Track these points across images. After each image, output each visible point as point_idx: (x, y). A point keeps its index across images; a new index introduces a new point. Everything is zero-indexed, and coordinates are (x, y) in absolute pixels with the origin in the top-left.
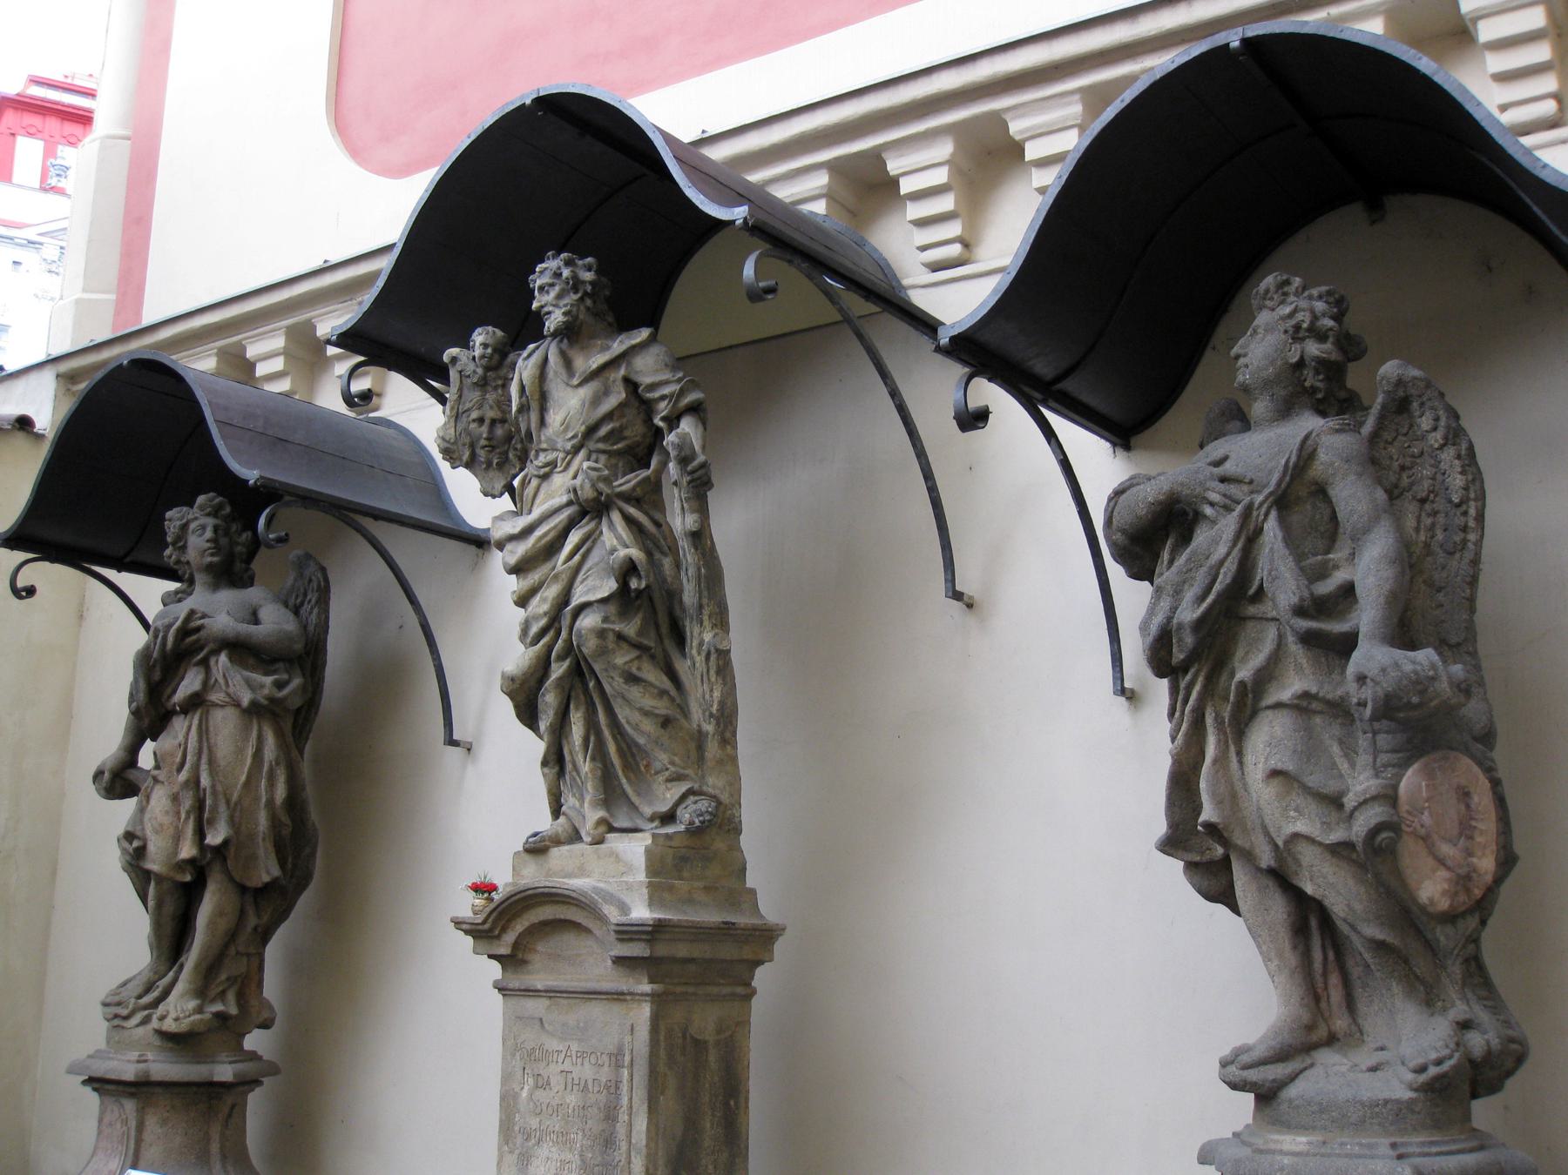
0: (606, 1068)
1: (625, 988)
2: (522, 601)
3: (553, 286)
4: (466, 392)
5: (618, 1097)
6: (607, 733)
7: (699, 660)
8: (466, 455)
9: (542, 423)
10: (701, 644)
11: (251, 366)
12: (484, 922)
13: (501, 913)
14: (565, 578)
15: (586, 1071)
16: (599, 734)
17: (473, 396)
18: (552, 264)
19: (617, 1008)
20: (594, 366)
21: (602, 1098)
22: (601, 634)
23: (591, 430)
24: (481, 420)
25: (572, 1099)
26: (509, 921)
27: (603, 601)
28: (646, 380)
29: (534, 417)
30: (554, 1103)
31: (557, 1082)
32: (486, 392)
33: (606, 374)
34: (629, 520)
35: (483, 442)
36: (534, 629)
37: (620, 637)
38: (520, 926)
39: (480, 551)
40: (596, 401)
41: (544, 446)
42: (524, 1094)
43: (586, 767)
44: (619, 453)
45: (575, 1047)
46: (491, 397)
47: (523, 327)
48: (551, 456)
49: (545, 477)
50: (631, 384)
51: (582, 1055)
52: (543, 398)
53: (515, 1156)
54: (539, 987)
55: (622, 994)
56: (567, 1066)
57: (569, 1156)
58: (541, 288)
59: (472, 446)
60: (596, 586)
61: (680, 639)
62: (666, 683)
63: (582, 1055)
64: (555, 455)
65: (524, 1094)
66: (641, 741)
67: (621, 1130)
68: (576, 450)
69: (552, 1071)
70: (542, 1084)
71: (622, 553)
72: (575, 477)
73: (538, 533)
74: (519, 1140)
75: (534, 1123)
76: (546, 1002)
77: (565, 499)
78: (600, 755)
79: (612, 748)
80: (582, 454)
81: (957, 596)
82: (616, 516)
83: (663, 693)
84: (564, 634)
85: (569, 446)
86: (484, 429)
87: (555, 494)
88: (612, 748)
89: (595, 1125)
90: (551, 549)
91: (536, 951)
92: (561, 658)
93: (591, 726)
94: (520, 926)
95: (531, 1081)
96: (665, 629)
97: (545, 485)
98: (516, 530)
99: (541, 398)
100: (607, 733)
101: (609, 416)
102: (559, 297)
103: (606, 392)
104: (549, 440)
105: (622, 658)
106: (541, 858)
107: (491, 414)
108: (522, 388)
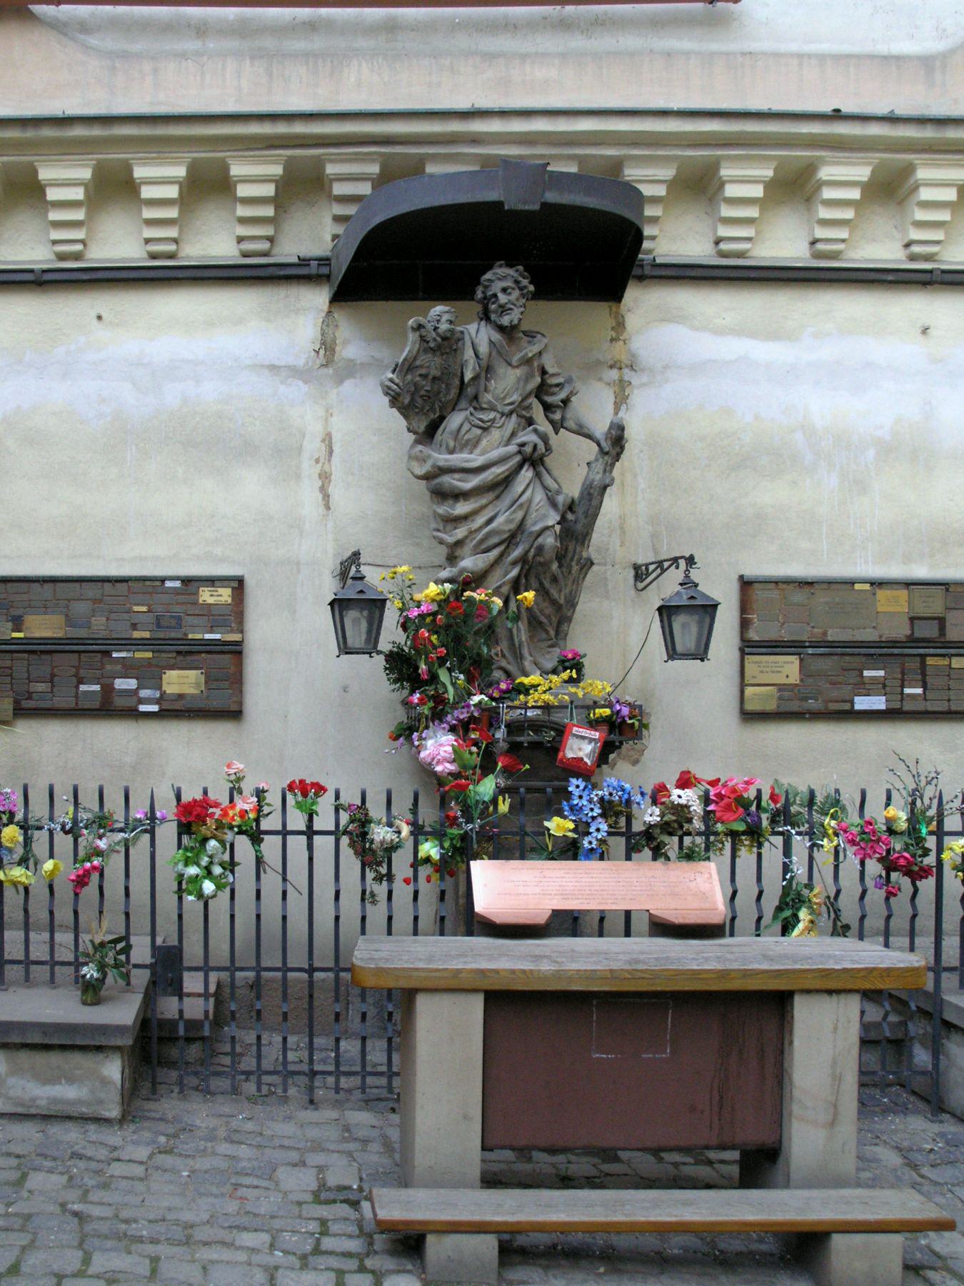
28: (550, 370)
35: (423, 393)
46: (438, 360)
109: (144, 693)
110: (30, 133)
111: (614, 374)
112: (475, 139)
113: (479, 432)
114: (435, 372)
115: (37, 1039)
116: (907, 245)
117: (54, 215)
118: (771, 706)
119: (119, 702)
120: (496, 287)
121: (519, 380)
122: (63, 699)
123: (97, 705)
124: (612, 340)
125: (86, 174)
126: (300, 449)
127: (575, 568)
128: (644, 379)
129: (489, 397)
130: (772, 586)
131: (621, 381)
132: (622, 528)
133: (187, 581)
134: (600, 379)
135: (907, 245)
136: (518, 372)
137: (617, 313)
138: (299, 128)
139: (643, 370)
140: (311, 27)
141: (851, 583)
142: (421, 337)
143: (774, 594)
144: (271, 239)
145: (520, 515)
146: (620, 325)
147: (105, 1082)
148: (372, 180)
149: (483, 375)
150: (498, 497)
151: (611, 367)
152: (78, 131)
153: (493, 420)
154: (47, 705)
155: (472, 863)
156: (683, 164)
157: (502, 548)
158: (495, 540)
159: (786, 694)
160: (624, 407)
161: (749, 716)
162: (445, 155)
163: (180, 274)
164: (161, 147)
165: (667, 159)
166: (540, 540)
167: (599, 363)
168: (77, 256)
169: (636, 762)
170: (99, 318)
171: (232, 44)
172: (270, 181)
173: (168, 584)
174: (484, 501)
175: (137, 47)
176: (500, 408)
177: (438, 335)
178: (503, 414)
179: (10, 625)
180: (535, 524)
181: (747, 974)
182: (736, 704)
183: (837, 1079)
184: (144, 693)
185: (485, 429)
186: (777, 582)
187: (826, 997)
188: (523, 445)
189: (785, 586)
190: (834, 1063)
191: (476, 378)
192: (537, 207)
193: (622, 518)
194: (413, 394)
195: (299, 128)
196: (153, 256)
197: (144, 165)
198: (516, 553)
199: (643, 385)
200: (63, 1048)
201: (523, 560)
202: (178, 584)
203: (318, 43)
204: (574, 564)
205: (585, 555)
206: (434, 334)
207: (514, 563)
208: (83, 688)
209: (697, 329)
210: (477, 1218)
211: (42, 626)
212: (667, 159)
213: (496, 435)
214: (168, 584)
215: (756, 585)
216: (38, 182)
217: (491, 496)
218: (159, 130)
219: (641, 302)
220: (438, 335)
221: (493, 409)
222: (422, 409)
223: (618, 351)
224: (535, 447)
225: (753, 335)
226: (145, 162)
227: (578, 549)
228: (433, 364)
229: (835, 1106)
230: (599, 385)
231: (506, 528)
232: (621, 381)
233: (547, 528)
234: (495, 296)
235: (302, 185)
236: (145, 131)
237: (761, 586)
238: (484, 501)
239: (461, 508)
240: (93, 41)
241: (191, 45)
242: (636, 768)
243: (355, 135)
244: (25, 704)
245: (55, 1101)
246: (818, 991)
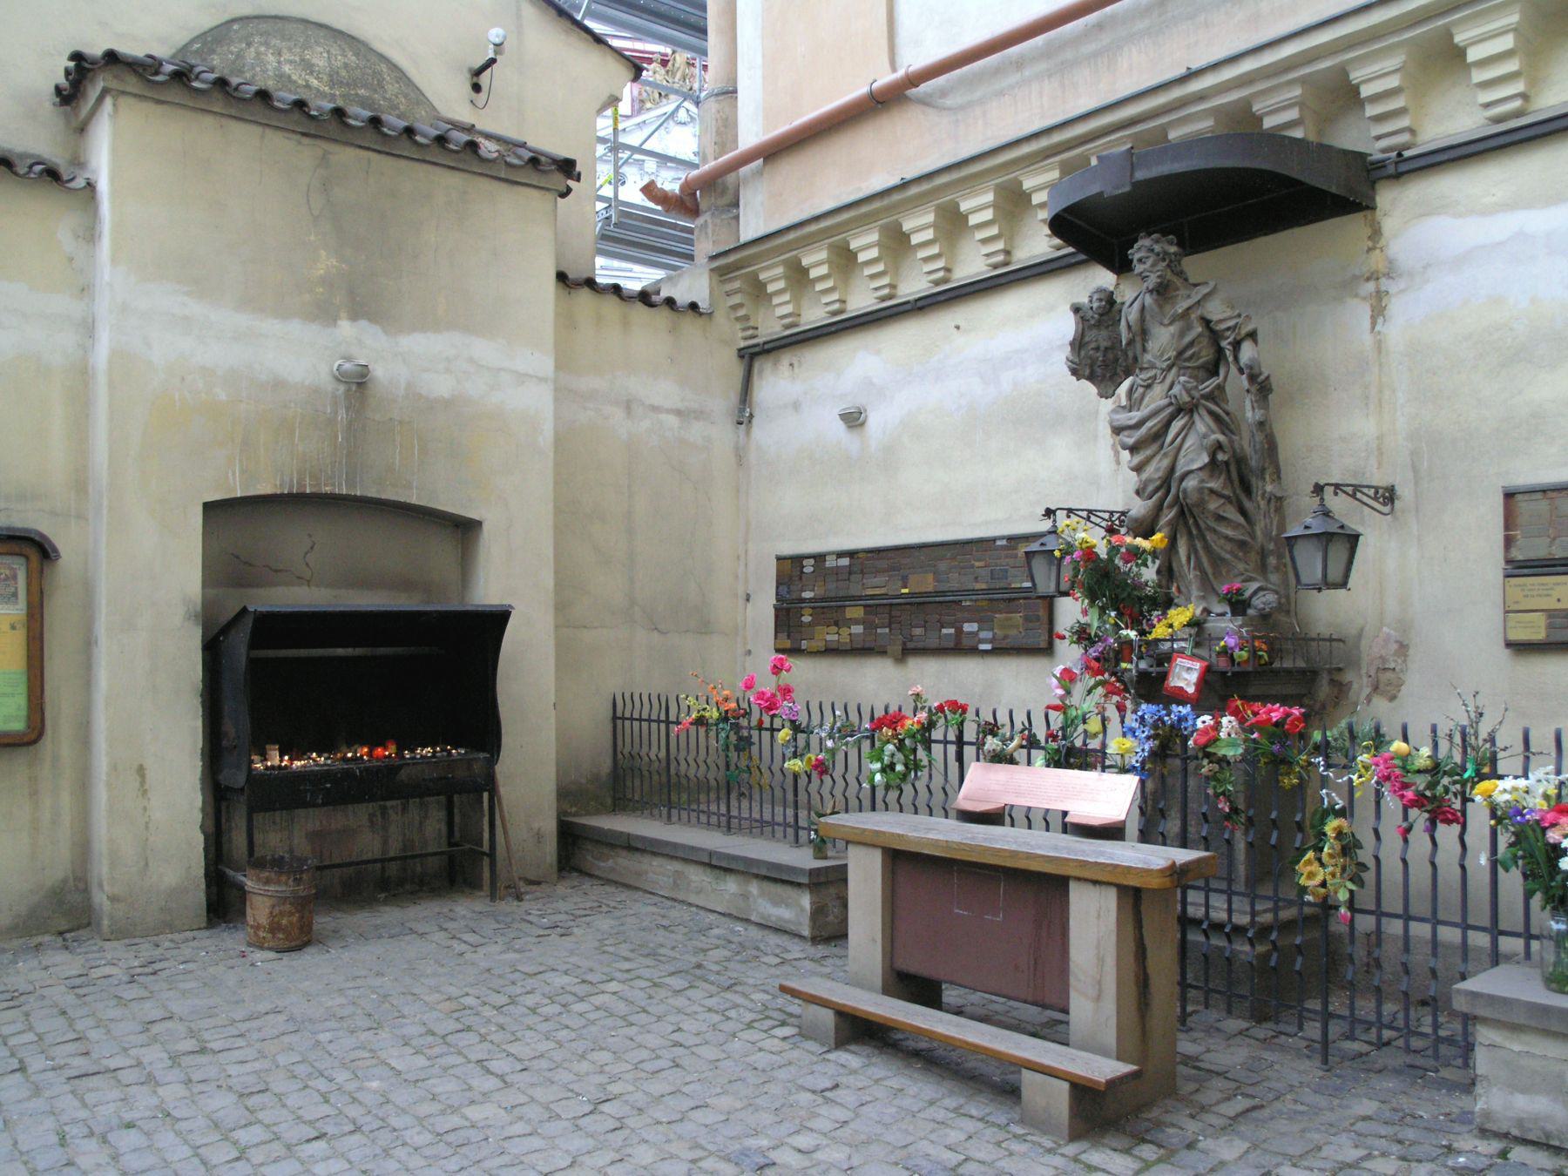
2: (1138, 469)
6: (1201, 552)
7: (1263, 503)
8: (1087, 372)
9: (1144, 350)
11: (805, 271)
14: (1172, 454)
16: (1196, 552)
18: (1144, 242)
22: (1200, 490)
24: (1097, 349)
27: (1200, 469)
28: (1214, 318)
29: (1139, 346)
34: (1211, 413)
36: (1150, 488)
37: (1212, 491)
40: (1182, 334)
43: (1192, 575)
44: (1198, 368)
46: (1104, 333)
48: (1151, 373)
49: (1148, 387)
50: (1207, 322)
58: (1140, 260)
59: (1091, 366)
60: (1194, 457)
61: (1247, 490)
62: (1241, 520)
68: (1170, 368)
71: (1213, 437)
72: (1171, 388)
73: (1149, 424)
77: (1166, 401)
78: (1199, 566)
79: (1205, 560)
80: (1174, 370)
82: (1203, 412)
83: (1237, 526)
84: (1173, 491)
85: (1164, 365)
86: (1100, 356)
87: (1156, 398)
88: (1205, 560)
90: (1158, 436)
92: (1171, 507)
93: (1192, 549)
96: (1236, 483)
98: (1133, 422)
100: (1201, 552)
101: (1191, 344)
102: (1153, 265)
103: (1189, 327)
105: (1213, 505)
108: (1129, 327)
109: (983, 635)
110: (886, 202)
111: (1370, 287)
112: (1201, 97)
114: (1104, 344)
115: (764, 872)
117: (1478, 76)
118: (1540, 635)
119: (966, 642)
121: (1173, 336)
122: (933, 642)
123: (952, 645)
124: (1370, 250)
126: (1097, 412)
128: (1402, 285)
129: (1148, 357)
130: (1539, 496)
131: (1378, 292)
132: (1379, 449)
133: (1010, 539)
134: (1356, 296)
136: (1172, 329)
137: (1373, 220)
138: (1057, 138)
139: (1400, 276)
140: (1100, 27)
141: (994, 540)
143: (1542, 505)
144: (1524, 96)
145: (1166, 462)
146: (1376, 233)
147: (802, 910)
148: (1515, 30)
149: (1138, 339)
151: (1368, 279)
152: (914, 191)
153: (1155, 377)
154: (920, 645)
155: (1137, 778)
156: (785, 263)
157: (1159, 494)
159: (1558, 621)
160: (1380, 320)
161: (1520, 648)
162: (1178, 120)
163: (901, 309)
164: (808, 242)
165: (1290, 83)
167: (1355, 278)
168: (841, 312)
169: (1393, 698)
170: (958, 328)
171: (1042, 66)
172: (1506, 32)
173: (999, 543)
174: (1149, 452)
175: (978, 94)
176: (1158, 364)
179: (900, 583)
181: (1030, 856)
182: (1501, 636)
183: (1101, 960)
184: (983, 635)
186: (1544, 491)
187: (1091, 886)
189: (1554, 494)
190: (1098, 947)
191: (1130, 342)
192: (1127, 189)
193: (1380, 438)
195: (1057, 138)
196: (1498, 120)
199: (1402, 291)
200: (784, 882)
202: (1004, 542)
203: (1106, 39)
208: (944, 631)
209: (1460, 216)
210: (813, 992)
211: (924, 582)
212: (1290, 83)
214: (999, 543)
215: (1519, 497)
216: (1456, 47)
217: (1154, 447)
218: (963, 171)
219: (1394, 203)
221: (1153, 367)
223: (1376, 261)
225: (1529, 205)
226: (965, 197)
228: (1101, 337)
229: (1099, 983)
230: (1355, 301)
232: (1378, 292)
233: (1191, 472)
235: (1013, 203)
236: (955, 175)
237: (1526, 497)
238: (1149, 452)
240: (949, 102)
241: (1014, 78)
242: (1393, 704)
243: (1068, 141)
244: (910, 645)
245: (780, 919)
246: (1086, 880)
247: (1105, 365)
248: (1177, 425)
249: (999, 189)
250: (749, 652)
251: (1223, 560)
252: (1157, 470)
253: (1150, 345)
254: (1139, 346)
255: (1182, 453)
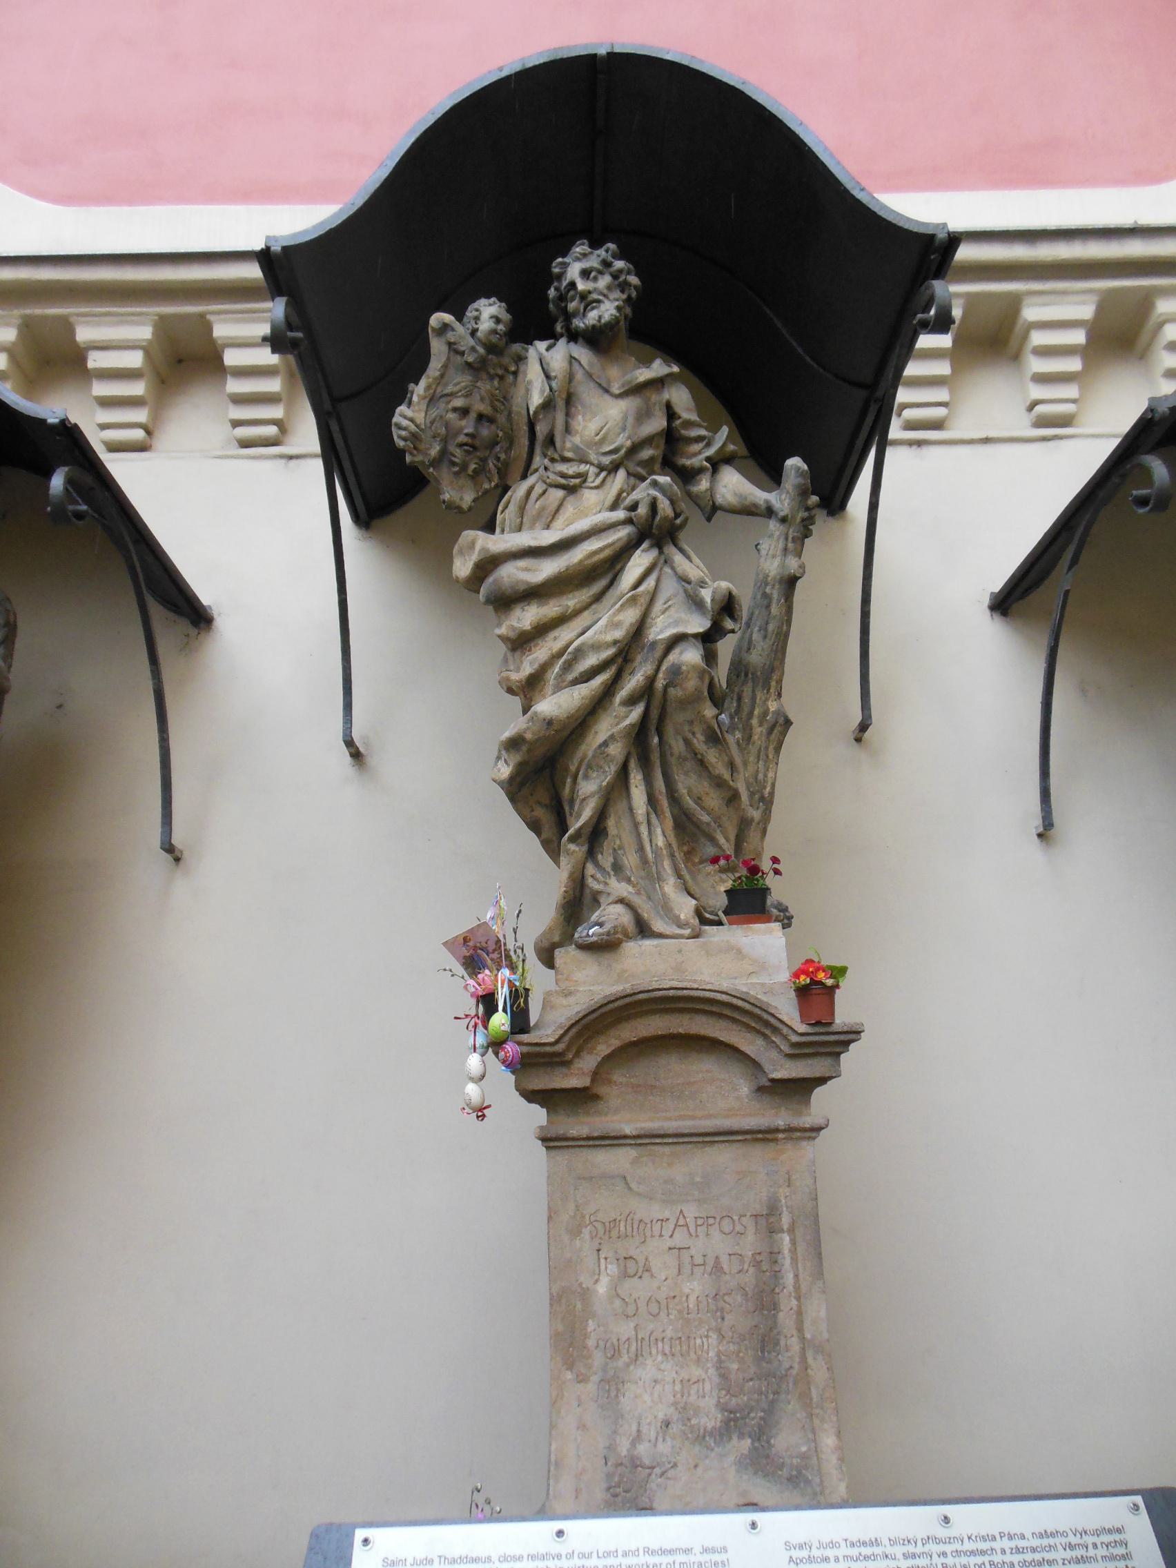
0: (750, 1237)
1: (781, 1123)
3: (592, 278)
4: (451, 371)
5: (777, 1275)
9: (568, 430)
10: (766, 713)
12: (557, 1042)
13: (586, 1027)
14: (643, 601)
15: (717, 1244)
17: (460, 381)
19: (757, 1156)
20: (642, 379)
21: (749, 1278)
23: (634, 449)
24: (464, 412)
25: (695, 1287)
26: (590, 1038)
29: (560, 418)
30: (661, 1296)
31: (663, 1266)
32: (477, 379)
33: (647, 393)
35: (462, 439)
38: (603, 1048)
39: (193, 631)
41: (569, 455)
42: (602, 1288)
45: (691, 1211)
46: (485, 386)
47: (536, 318)
51: (706, 1221)
52: (569, 400)
53: (591, 1387)
54: (628, 1130)
55: (777, 1130)
56: (680, 1238)
57: (697, 1372)
63: (706, 1221)
64: (583, 468)
65: (602, 1288)
66: (706, 818)
67: (786, 1320)
68: (613, 468)
69: (656, 1252)
70: (630, 1268)
74: (598, 1359)
75: (625, 1330)
76: (632, 1153)
80: (621, 474)
81: (169, 848)
89: (738, 1319)
91: (610, 1082)
92: (631, 701)
94: (603, 1048)
95: (613, 1269)
97: (571, 499)
99: (564, 400)
104: (576, 449)
106: (606, 958)
107: (480, 407)
113: (560, 493)
116: (1031, 408)
120: (574, 271)
125: (145, 333)
127: (758, 731)
135: (1031, 408)
142: (450, 344)
145: (630, 616)
149: (561, 404)
150: (598, 598)
158: (591, 660)
166: (673, 657)
176: (593, 457)
177: (480, 341)
178: (601, 468)
180: (661, 632)
185: (571, 490)
188: (634, 507)
191: (548, 405)
194: (445, 441)
197: (225, 321)
198: (634, 682)
201: (646, 692)
204: (755, 722)
205: (773, 706)
206: (472, 342)
207: (631, 701)
213: (590, 497)
220: (480, 341)
222: (464, 467)
224: (653, 506)
227: (760, 695)
231: (609, 638)
234: (573, 285)
239: (527, 617)
247: (471, 447)
248: (640, 561)
249: (163, 326)
250: (655, 1381)
251: (697, 825)
252: (615, 625)
253: (579, 422)
254: (560, 418)
255: (658, 606)
